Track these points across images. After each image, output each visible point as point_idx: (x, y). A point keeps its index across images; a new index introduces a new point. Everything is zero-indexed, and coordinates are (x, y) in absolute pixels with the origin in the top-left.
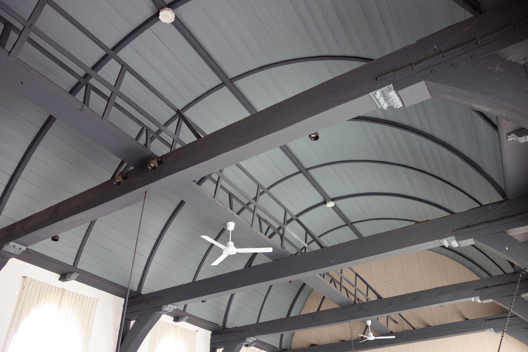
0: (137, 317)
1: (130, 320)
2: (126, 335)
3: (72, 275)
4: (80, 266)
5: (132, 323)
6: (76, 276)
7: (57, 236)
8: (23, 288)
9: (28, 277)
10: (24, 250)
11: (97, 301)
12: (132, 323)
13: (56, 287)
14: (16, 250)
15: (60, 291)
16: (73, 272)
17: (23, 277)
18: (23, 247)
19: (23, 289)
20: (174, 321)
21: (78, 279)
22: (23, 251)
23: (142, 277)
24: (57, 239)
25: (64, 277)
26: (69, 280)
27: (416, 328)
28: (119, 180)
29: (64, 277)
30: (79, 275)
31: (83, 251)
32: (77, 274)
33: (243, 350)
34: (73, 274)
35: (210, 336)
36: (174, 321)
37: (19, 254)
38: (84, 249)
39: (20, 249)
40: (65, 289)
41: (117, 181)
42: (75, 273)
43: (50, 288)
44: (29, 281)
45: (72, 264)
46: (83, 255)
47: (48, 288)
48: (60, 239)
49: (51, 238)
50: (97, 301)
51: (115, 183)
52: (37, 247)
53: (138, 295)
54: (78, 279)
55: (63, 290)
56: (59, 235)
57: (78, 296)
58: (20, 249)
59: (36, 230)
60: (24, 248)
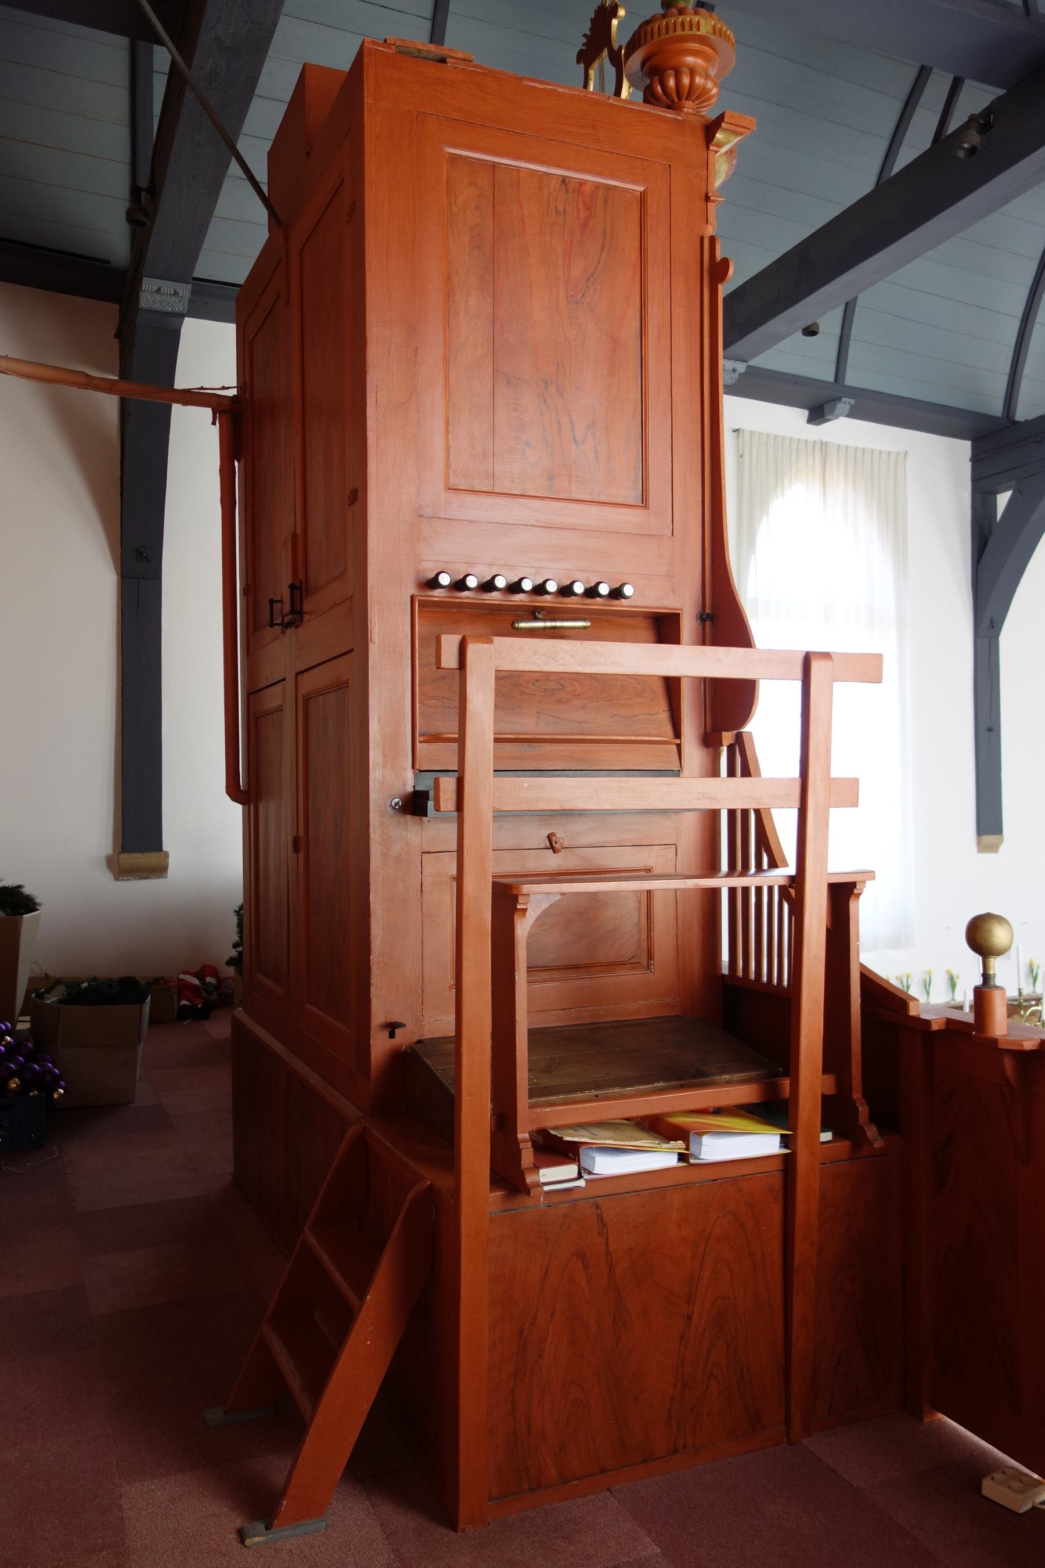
0: (1014, 483)
1: (994, 493)
2: (990, 532)
3: (836, 405)
4: (851, 379)
5: (1003, 499)
6: (848, 407)
7: (816, 324)
8: (741, 456)
9: (743, 430)
10: (742, 372)
11: (904, 460)
12: (1003, 499)
13: (806, 441)
14: (725, 377)
15: (818, 446)
16: (839, 399)
17: (734, 431)
18: (740, 366)
19: (741, 459)
20: (810, 420)
21: (853, 414)
22: (740, 374)
23: (1010, 374)
24: (815, 330)
25: (818, 414)
26: (831, 420)
27: (425, 1041)
28: (974, 143)
29: (818, 414)
30: (853, 402)
31: (852, 338)
32: (848, 400)
33: (434, 402)
34: (840, 401)
35: (970, 463)
36: (810, 420)
37: (734, 382)
38: (853, 332)
39: (734, 370)
40: (826, 443)
41: (966, 146)
42: (844, 399)
43: (794, 446)
44: (747, 437)
45: (830, 377)
46: (854, 350)
47: (790, 445)
48: (821, 330)
49: (801, 331)
50: (904, 460)
51: (961, 154)
52: (771, 359)
53: (1008, 427)
54: (855, 413)
55: (824, 446)
56: (820, 321)
57: (860, 454)
58: (734, 370)
59: (768, 321)
60: (741, 367)
